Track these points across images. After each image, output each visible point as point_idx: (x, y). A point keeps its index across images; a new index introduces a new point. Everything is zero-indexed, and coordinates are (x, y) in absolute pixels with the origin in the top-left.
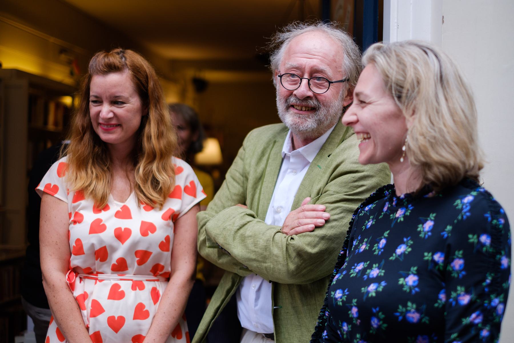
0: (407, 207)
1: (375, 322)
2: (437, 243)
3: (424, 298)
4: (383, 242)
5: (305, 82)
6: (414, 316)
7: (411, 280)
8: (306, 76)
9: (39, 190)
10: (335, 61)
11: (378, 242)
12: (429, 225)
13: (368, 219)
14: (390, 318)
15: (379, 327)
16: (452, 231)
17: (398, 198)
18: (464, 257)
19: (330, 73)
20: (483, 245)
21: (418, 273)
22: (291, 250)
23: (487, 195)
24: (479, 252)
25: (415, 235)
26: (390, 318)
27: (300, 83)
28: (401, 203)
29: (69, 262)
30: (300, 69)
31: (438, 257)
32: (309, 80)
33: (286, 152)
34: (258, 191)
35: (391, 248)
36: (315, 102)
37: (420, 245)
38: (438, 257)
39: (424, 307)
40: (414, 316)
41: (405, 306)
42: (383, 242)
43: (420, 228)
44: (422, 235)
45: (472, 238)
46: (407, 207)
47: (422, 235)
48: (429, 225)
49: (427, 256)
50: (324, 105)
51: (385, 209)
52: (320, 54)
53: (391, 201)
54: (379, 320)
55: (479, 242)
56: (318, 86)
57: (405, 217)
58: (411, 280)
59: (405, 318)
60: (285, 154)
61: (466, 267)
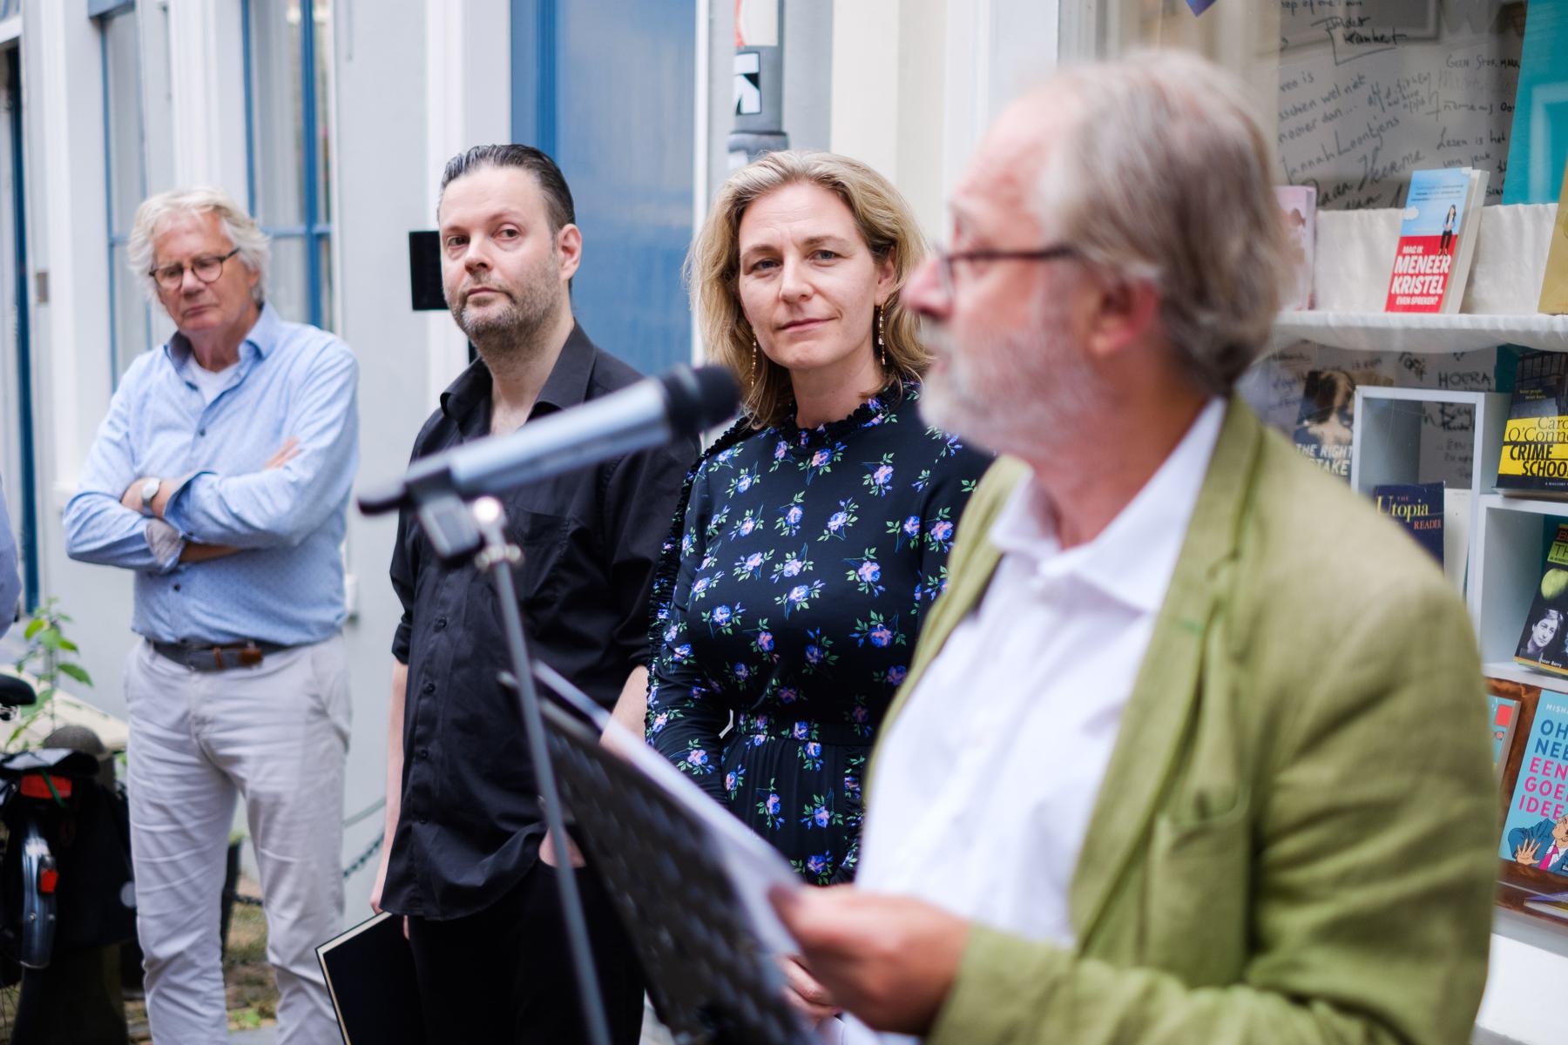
0: (832, 447)
1: (813, 655)
4: (795, 513)
11: (785, 514)
12: (883, 474)
13: (737, 476)
15: (822, 662)
25: (861, 494)
37: (873, 510)
41: (868, 619)
42: (795, 513)
44: (875, 491)
46: (832, 447)
47: (875, 491)
48: (883, 474)
49: (892, 527)
51: (780, 454)
54: (822, 649)
58: (869, 571)
59: (868, 639)
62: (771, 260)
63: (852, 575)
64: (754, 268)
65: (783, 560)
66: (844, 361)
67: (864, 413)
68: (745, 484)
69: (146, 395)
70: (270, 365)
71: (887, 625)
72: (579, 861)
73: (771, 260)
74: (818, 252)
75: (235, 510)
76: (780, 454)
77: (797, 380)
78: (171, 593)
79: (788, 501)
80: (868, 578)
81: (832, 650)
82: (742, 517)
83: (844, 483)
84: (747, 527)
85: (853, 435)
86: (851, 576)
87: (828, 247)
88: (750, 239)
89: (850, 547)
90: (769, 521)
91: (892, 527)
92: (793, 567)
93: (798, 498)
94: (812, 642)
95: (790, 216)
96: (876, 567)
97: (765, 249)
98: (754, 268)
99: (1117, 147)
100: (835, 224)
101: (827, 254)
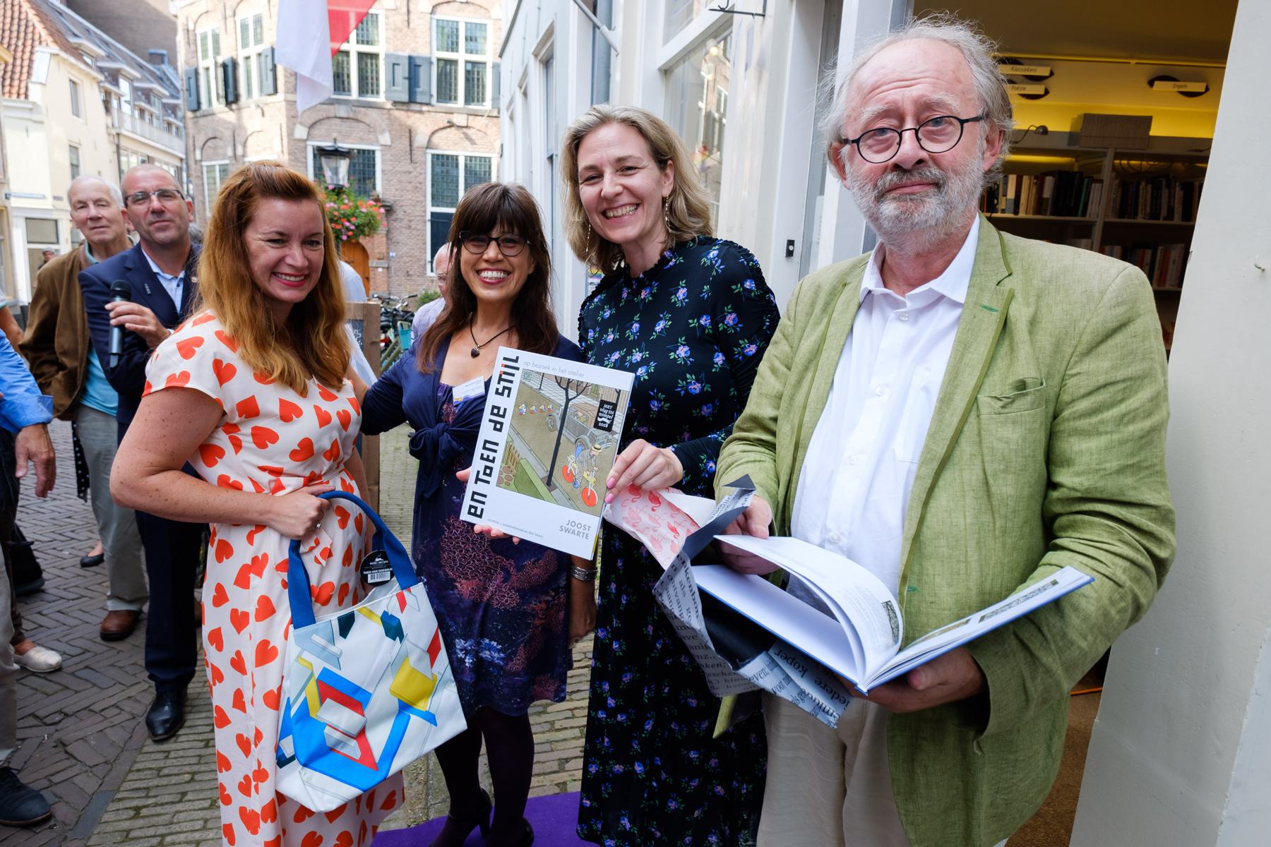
0: (651, 285)
1: (655, 406)
2: (697, 307)
3: (700, 366)
4: (636, 326)
5: (908, 136)
6: (696, 388)
7: (683, 351)
8: (909, 124)
9: (539, 800)
10: (959, 81)
11: (630, 328)
12: (682, 293)
13: (603, 309)
14: (672, 396)
15: (661, 409)
16: (711, 290)
17: (638, 279)
18: (735, 310)
19: (956, 105)
20: (750, 291)
21: (688, 343)
22: (77, 273)
23: (729, 244)
24: (749, 299)
25: (671, 308)
26: (672, 396)
27: (899, 144)
28: (642, 285)
29: (211, 435)
30: (895, 113)
31: (705, 321)
32: (917, 131)
33: (871, 287)
34: (810, 375)
35: (647, 327)
36: (935, 171)
37: (679, 315)
38: (705, 321)
39: (703, 375)
40: (696, 388)
41: (685, 379)
42: (636, 326)
43: (673, 299)
44: (679, 304)
45: (737, 288)
46: (651, 285)
47: (679, 304)
48: (682, 293)
49: (693, 323)
50: (956, 173)
51: (625, 295)
52: (928, 74)
53: (629, 286)
54: (659, 401)
55: (745, 289)
56: (932, 137)
57: (652, 295)
58: (683, 351)
59: (687, 391)
60: (870, 292)
61: (740, 319)
62: (596, 175)
63: (672, 355)
64: (587, 180)
65: (631, 354)
66: (644, 236)
67: (663, 260)
68: (607, 314)
69: (395, 103)
70: (399, 213)
71: (698, 380)
72: (477, 529)
73: (596, 175)
74: (624, 167)
75: (1011, 313)
76: (625, 295)
77: (624, 247)
78: (1222, 828)
79: (630, 322)
80: (683, 355)
81: (666, 401)
82: (607, 333)
83: (661, 303)
84: (611, 337)
85: (661, 275)
86: (672, 355)
87: (629, 164)
88: (584, 161)
89: (669, 340)
90: (622, 333)
91: (693, 323)
92: (637, 356)
93: (636, 318)
94: (653, 398)
95: (609, 144)
96: (687, 348)
97: (591, 168)
98: (587, 180)
99: (346, 307)
100: (634, 148)
101: (630, 168)
